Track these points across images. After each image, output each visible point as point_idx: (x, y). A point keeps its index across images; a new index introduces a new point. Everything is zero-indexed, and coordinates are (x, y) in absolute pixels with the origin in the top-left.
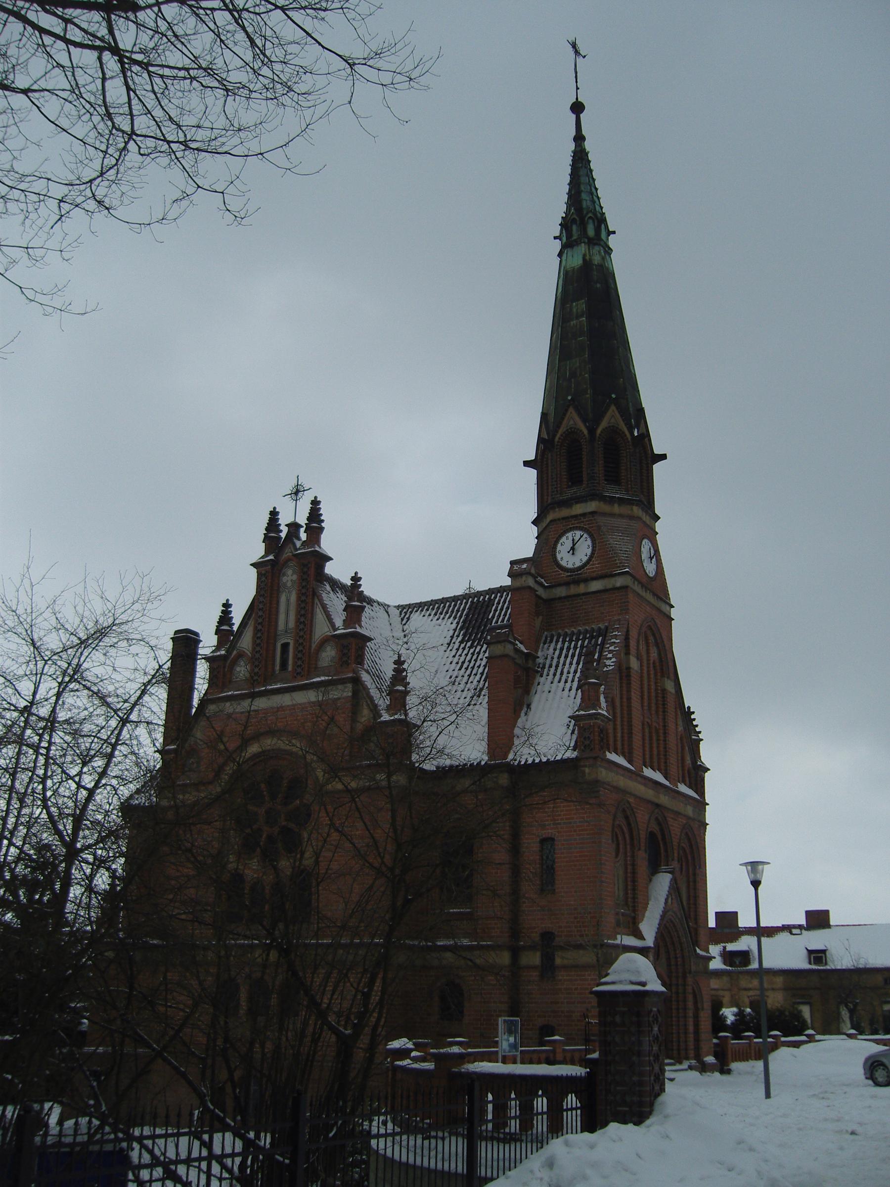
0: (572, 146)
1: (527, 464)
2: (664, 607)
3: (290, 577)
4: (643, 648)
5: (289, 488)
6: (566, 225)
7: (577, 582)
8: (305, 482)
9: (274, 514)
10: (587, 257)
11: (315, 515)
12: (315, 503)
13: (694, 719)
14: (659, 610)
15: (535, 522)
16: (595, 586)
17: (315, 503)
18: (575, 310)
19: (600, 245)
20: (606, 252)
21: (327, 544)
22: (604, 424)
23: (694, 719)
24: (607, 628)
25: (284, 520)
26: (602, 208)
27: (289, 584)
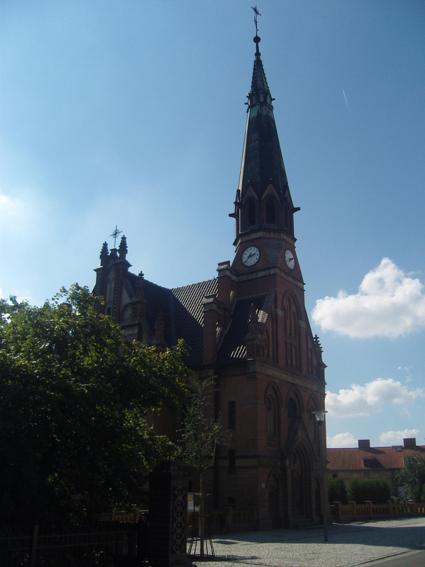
0: (254, 58)
1: (230, 215)
2: (299, 284)
3: (112, 275)
4: (286, 303)
5: (112, 232)
6: (250, 97)
7: (252, 273)
8: (120, 229)
9: (105, 245)
10: (260, 112)
12: (124, 238)
13: (319, 341)
14: (297, 286)
16: (261, 274)
17: (124, 238)
18: (253, 138)
19: (266, 106)
20: (269, 109)
21: (129, 258)
22: (266, 193)
23: (319, 341)
24: (266, 295)
25: (110, 247)
26: (268, 88)
27: (111, 279)
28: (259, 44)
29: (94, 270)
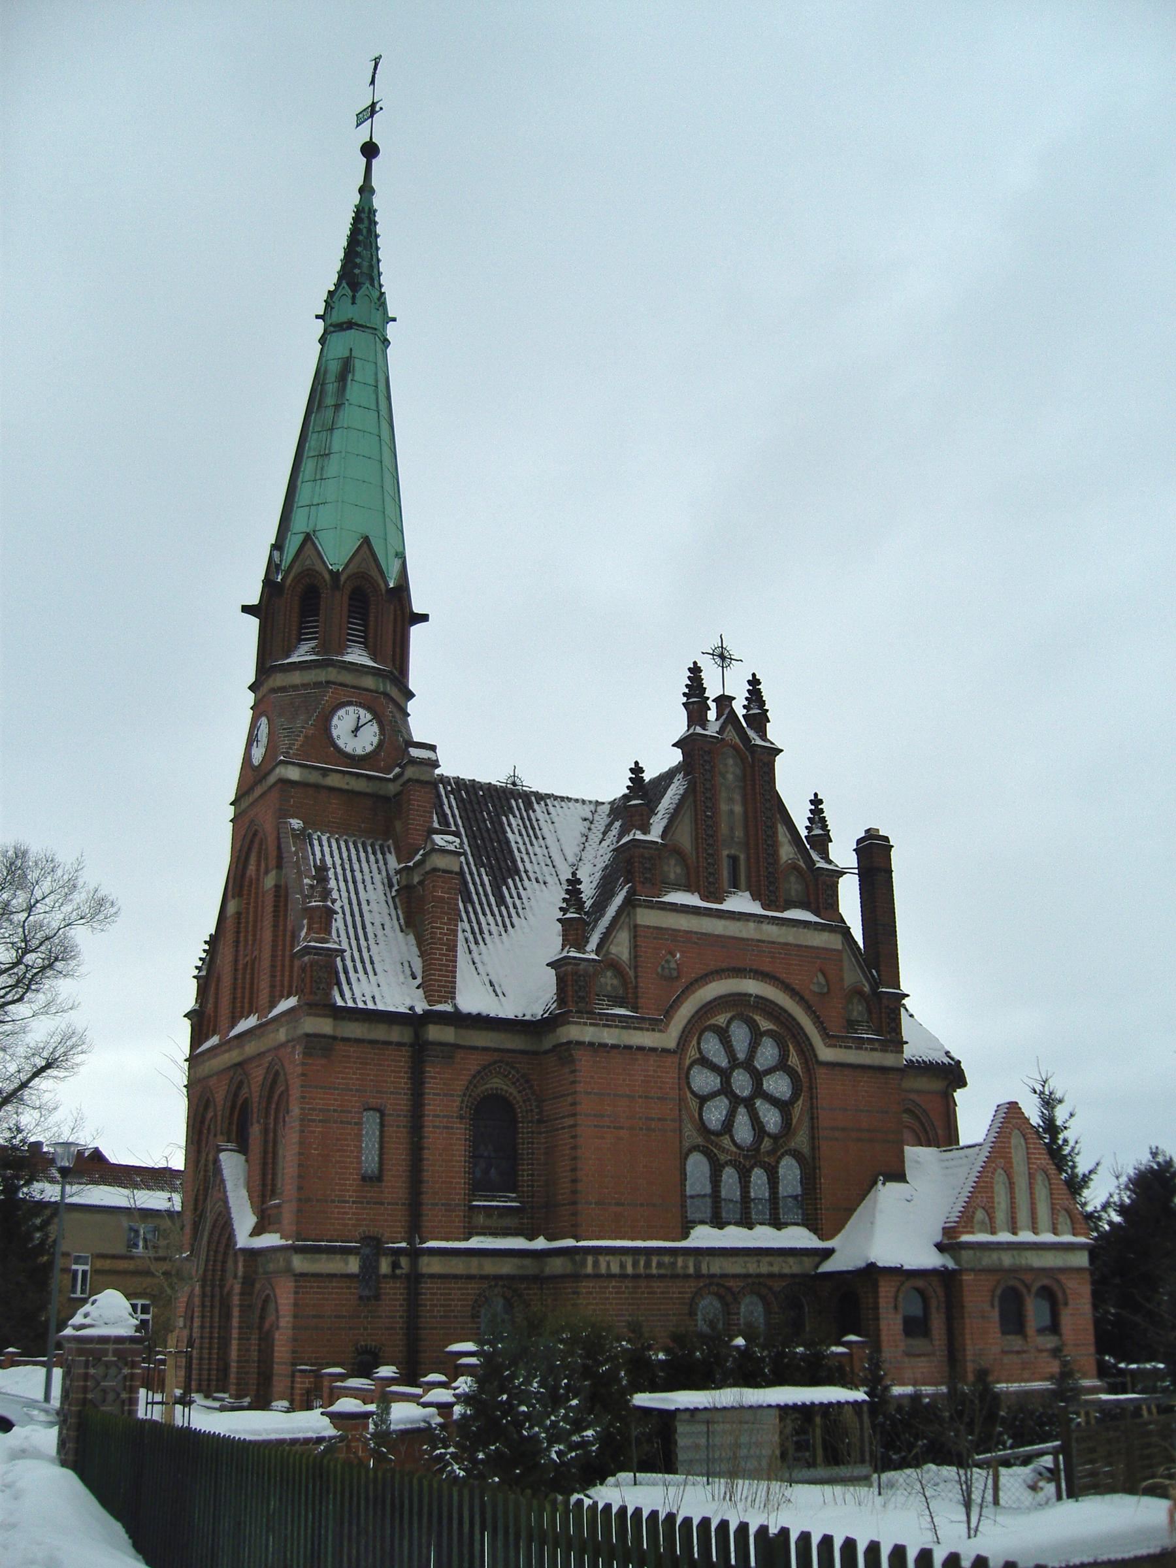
0: (356, 199)
1: (246, 609)
11: (755, 694)
15: (251, 688)
28: (374, 162)
29: (548, 965)
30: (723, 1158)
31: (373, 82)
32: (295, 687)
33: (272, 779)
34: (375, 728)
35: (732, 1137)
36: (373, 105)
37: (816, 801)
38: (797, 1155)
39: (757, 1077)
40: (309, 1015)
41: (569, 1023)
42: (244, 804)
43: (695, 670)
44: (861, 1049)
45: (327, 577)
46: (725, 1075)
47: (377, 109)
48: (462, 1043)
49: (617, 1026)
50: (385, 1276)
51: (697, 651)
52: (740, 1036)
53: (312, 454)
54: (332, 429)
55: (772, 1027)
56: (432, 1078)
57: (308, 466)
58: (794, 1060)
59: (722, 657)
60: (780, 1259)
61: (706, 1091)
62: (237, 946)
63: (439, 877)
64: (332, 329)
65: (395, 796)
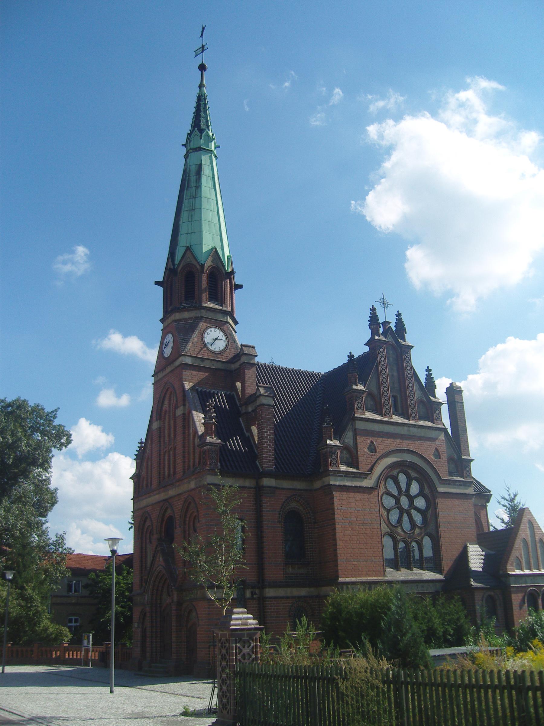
1: (157, 283)
30: (399, 538)
31: (202, 35)
32: (186, 319)
33: (177, 363)
34: (206, 341)
35: (402, 527)
36: (203, 46)
37: (428, 370)
38: (430, 536)
39: (411, 499)
40: (209, 474)
41: (329, 475)
42: (161, 375)
43: (373, 310)
44: (455, 485)
45: (198, 267)
46: (397, 500)
47: (205, 48)
48: (279, 486)
49: (350, 477)
50: (249, 599)
51: (373, 301)
52: (402, 478)
53: (186, 209)
54: (195, 198)
55: (416, 475)
56: (265, 503)
57: (184, 215)
58: (427, 491)
59: (384, 303)
60: (426, 584)
61: (390, 505)
62: (160, 444)
63: (265, 408)
64: (191, 151)
65: (235, 370)
